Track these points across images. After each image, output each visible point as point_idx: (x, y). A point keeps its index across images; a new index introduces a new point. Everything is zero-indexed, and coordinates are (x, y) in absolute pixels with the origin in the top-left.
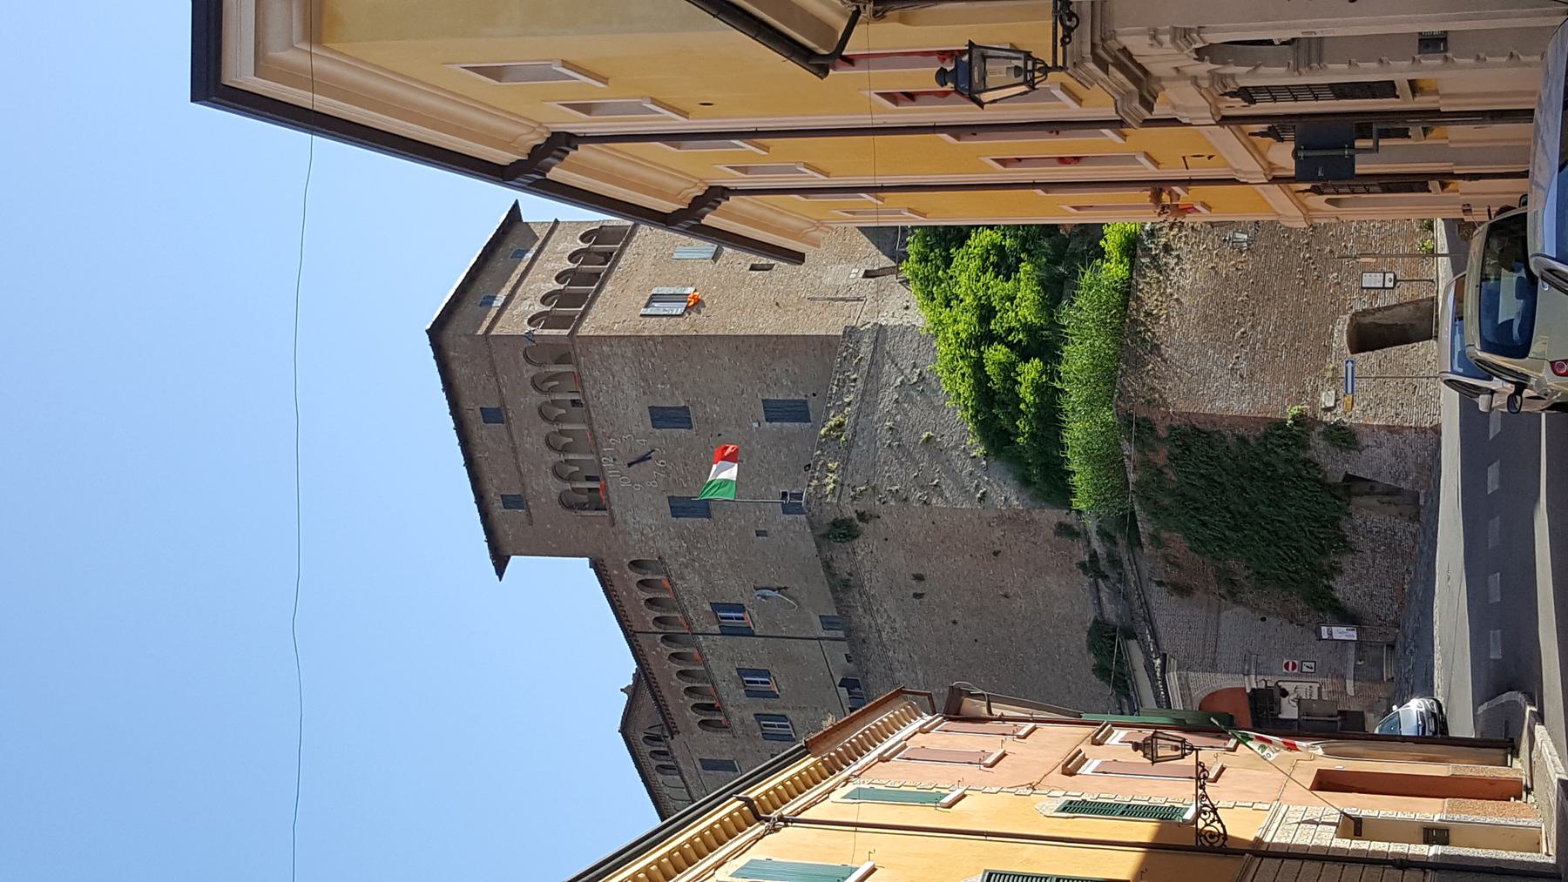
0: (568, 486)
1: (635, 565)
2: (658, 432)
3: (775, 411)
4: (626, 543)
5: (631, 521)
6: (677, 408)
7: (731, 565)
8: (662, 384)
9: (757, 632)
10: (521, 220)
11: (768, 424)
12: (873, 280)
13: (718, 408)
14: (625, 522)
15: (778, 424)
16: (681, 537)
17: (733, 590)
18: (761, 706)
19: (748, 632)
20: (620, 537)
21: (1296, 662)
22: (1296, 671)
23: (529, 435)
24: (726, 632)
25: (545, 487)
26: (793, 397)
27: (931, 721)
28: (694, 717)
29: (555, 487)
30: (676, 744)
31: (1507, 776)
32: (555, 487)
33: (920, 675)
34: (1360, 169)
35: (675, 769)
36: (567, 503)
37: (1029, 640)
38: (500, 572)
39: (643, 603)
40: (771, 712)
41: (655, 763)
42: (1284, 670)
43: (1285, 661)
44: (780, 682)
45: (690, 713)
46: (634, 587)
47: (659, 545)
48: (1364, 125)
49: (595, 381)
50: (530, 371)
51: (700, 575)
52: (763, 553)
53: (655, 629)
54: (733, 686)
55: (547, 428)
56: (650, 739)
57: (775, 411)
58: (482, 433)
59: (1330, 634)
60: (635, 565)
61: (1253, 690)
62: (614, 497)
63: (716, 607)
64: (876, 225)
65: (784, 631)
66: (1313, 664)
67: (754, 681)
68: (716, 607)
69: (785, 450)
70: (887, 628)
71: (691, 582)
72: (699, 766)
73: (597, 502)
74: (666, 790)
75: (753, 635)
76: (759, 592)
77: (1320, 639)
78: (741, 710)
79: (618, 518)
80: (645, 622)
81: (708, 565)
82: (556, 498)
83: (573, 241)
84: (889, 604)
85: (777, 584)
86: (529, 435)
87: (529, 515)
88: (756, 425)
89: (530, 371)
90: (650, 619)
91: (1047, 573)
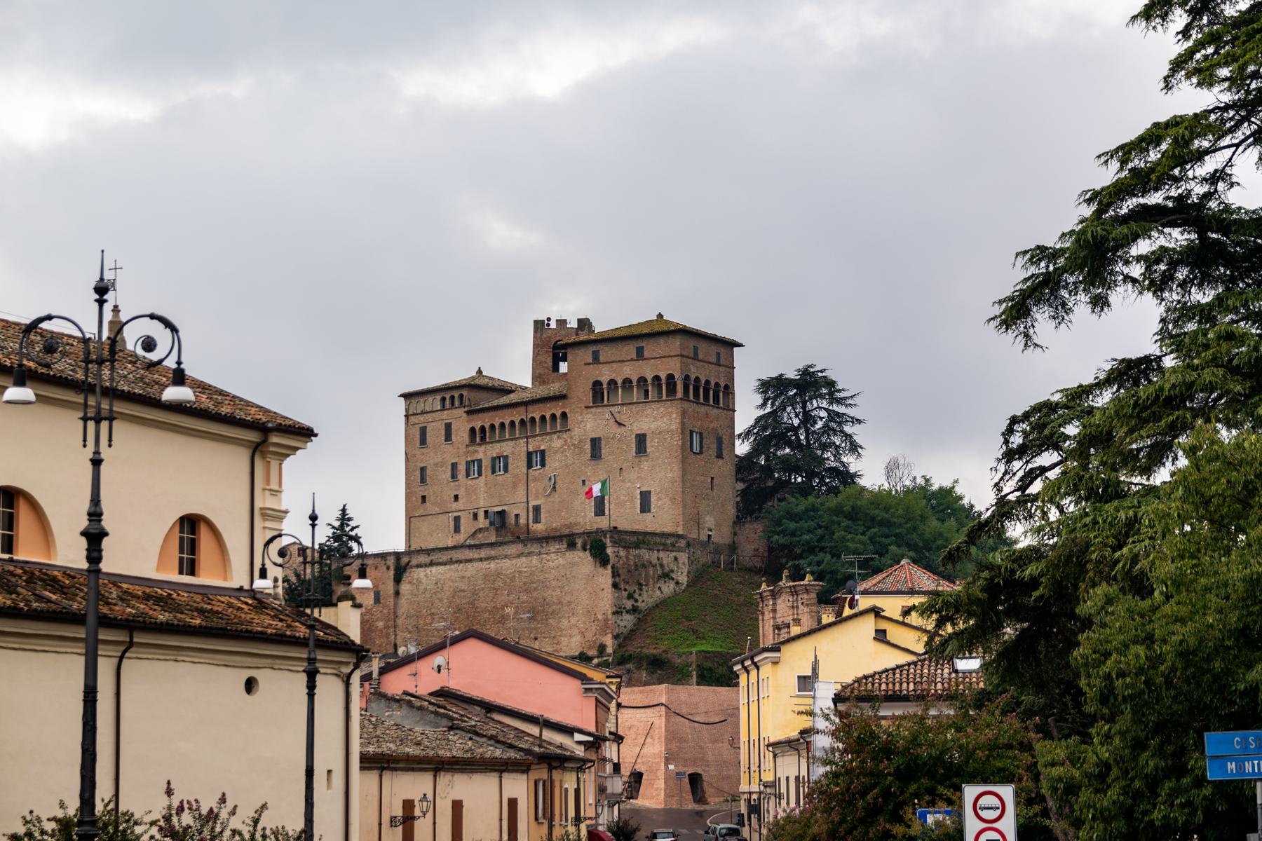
0: (605, 386)
1: (564, 415)
2: (634, 436)
3: (645, 497)
9: (530, 471)
15: (639, 497)
16: (581, 441)
17: (553, 463)
18: (486, 463)
19: (529, 466)
20: (579, 410)
24: (529, 455)
26: (653, 506)
27: (612, 691)
28: (478, 425)
29: (605, 380)
32: (605, 380)
34: (752, 816)
35: (443, 409)
36: (597, 384)
41: (448, 396)
44: (501, 477)
46: (552, 412)
48: (759, 816)
49: (659, 408)
53: (529, 417)
54: (497, 451)
55: (634, 380)
57: (645, 497)
58: (630, 350)
62: (600, 410)
63: (543, 452)
64: (743, 737)
65: (531, 485)
67: (502, 463)
68: (543, 452)
69: (626, 499)
70: (549, 558)
71: (556, 443)
72: (447, 421)
76: (553, 478)
78: (485, 453)
79: (589, 410)
80: (533, 412)
82: (599, 379)
84: (561, 561)
85: (557, 487)
87: (589, 364)
90: (534, 415)
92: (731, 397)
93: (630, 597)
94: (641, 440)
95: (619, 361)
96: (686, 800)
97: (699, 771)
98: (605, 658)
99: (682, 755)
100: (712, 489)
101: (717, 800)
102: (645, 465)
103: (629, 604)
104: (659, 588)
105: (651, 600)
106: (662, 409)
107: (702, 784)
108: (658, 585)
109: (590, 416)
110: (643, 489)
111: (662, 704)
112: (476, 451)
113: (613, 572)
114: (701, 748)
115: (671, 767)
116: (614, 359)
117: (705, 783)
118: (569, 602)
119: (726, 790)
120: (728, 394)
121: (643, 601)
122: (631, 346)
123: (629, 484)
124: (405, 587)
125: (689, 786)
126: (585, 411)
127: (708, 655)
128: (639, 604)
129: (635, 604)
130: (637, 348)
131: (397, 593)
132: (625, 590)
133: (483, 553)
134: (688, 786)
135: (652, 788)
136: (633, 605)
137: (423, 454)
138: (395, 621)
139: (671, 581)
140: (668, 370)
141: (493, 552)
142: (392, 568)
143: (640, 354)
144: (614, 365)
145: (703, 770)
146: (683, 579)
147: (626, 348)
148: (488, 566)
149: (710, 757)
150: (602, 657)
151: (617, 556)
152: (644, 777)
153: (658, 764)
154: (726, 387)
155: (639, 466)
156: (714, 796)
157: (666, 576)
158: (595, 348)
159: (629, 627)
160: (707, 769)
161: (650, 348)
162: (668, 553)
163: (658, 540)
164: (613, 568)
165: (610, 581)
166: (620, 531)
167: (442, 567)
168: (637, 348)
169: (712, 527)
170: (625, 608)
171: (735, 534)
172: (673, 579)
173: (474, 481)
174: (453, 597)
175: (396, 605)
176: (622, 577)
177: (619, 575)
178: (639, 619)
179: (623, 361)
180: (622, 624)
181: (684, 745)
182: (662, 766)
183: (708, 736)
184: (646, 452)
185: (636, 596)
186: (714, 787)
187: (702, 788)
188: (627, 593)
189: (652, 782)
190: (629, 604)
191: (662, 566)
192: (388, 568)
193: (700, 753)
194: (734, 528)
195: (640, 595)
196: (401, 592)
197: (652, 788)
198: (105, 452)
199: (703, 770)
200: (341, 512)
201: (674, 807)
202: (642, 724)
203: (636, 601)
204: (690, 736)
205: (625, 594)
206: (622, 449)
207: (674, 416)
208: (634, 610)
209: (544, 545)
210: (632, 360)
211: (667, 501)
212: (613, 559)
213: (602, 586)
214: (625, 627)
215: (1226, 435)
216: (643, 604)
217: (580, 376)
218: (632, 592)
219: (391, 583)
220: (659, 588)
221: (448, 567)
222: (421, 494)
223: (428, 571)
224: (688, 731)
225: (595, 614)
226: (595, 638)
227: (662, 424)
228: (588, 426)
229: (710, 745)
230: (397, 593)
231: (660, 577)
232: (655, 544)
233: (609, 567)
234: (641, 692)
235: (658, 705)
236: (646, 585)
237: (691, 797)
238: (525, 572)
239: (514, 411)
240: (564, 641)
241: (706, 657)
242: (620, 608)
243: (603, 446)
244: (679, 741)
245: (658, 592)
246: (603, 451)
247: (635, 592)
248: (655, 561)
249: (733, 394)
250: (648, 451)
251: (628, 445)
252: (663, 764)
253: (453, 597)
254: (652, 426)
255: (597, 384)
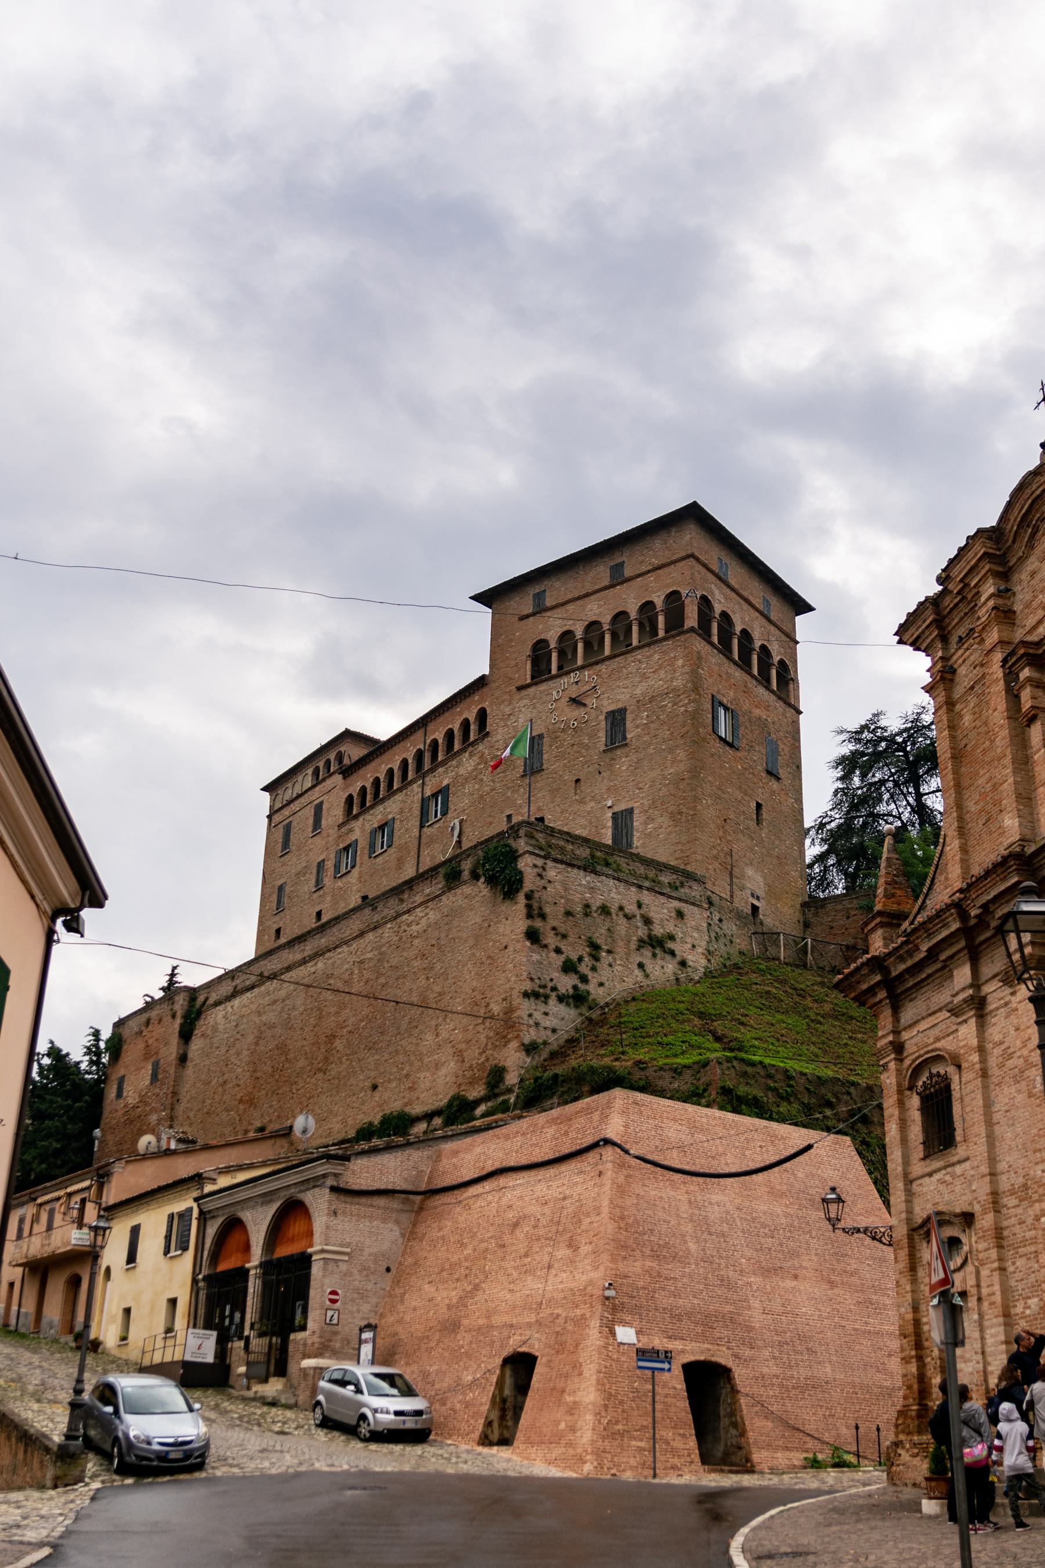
1: (482, 715)
2: (602, 717)
4: (503, 702)
5: (521, 704)
6: (625, 731)
7: (481, 797)
8: (648, 716)
10: (797, 615)
11: (610, 815)
12: (750, 912)
13: (624, 768)
14: (522, 699)
15: (610, 824)
18: (363, 844)
20: (506, 697)
21: (339, 1304)
22: (328, 1303)
23: (600, 606)
24: (424, 803)
25: (551, 628)
26: (636, 835)
28: (355, 789)
30: (338, 778)
31: (802, 1486)
32: (552, 637)
33: (369, 955)
36: (541, 645)
37: (397, 1052)
38: (478, 598)
39: (450, 726)
40: (359, 853)
42: (329, 1290)
43: (339, 1291)
45: (359, 785)
46: (464, 716)
47: (500, 731)
50: (659, 601)
51: (473, 771)
52: (491, 823)
53: (428, 741)
56: (340, 757)
58: (600, 573)
59: (366, 1341)
60: (482, 715)
61: (310, 1256)
62: (543, 687)
66: (335, 1321)
70: (411, 918)
73: (540, 671)
74: (300, 778)
75: (422, 826)
76: (457, 825)
77: (361, 1330)
78: (360, 830)
79: (524, 693)
80: (434, 733)
81: (481, 776)
83: (780, 653)
84: (433, 916)
86: (600, 606)
88: (609, 803)
89: (659, 601)
91: (457, 1061)
92: (791, 686)
93: (569, 967)
94: (617, 719)
95: (579, 598)
96: (674, 1452)
97: (723, 1358)
98: (501, 1098)
99: (664, 1300)
100: (759, 821)
101: (781, 1458)
102: (623, 762)
103: (566, 983)
104: (641, 966)
105: (619, 987)
106: (657, 656)
107: (735, 1402)
108: (639, 959)
109: (525, 701)
110: (616, 809)
111: (607, 1142)
112: (351, 830)
113: (529, 907)
114: (725, 1282)
115: (626, 1334)
116: (570, 596)
117: (743, 1401)
118: (440, 994)
119: (810, 1428)
120: (787, 684)
121: (601, 984)
122: (601, 568)
123: (592, 804)
124: (196, 1045)
125: (685, 1404)
126: (517, 696)
127: (750, 1070)
128: (592, 987)
129: (582, 987)
130: (612, 568)
131: (183, 1059)
132: (558, 951)
133: (308, 948)
134: (683, 1404)
135: (559, 1402)
136: (575, 987)
137: (284, 864)
138: (172, 1109)
139: (668, 957)
140: (667, 586)
141: (322, 941)
142: (179, 1014)
143: (618, 579)
144: (570, 607)
145: (736, 1356)
146: (698, 961)
147: (592, 574)
148: (313, 970)
149: (757, 1317)
150: (496, 1096)
151: (540, 875)
152: (539, 1370)
153: (581, 1322)
154: (783, 666)
155: (610, 767)
156: (769, 1446)
157: (657, 944)
158: (537, 589)
159: (563, 1036)
160: (748, 1353)
161: (633, 561)
162: (662, 899)
163: (641, 870)
164: (529, 896)
165: (521, 925)
166: (552, 832)
167: (248, 994)
168: (612, 568)
169: (760, 893)
170: (554, 989)
171: (806, 925)
172: (672, 953)
173: (344, 879)
174: (257, 1044)
175: (178, 1080)
176: (552, 922)
177: (543, 916)
178: (590, 1020)
179: (587, 595)
180: (547, 1022)
181: (673, 1269)
182: (593, 1335)
183: (748, 1253)
184: (625, 738)
185: (584, 969)
186: (768, 1415)
187: (734, 1412)
188: (562, 958)
189: (560, 1385)
190: (566, 983)
191: (647, 921)
192: (174, 1016)
193: (727, 1301)
194: (804, 914)
195: (594, 969)
196: (190, 1055)
197: (559, 1402)
198: (200, 1142)
199: (736, 1356)
200: (168, 978)
201: (628, 1476)
202: (546, 1210)
203: (584, 979)
204: (692, 1246)
205: (558, 960)
206: (580, 744)
207: (680, 662)
208: (578, 998)
209: (406, 896)
210: (606, 588)
211: (664, 820)
212: (530, 882)
213: (504, 941)
214: (554, 1031)
215: (916, 1438)
216: (601, 991)
217: (511, 641)
218: (574, 957)
219: (175, 1040)
220: (641, 966)
221: (256, 990)
222: (276, 927)
223: (229, 1009)
224: (689, 1228)
225: (488, 1005)
226: (483, 1059)
227: (657, 682)
228: (521, 721)
229: (756, 1280)
230: (183, 1059)
231: (642, 944)
232: (632, 873)
233: (521, 898)
234: (554, 1121)
235: (595, 1146)
236: (609, 952)
237: (692, 1443)
238: (370, 959)
239: (407, 743)
240: (425, 1079)
241: (745, 1074)
242: (544, 987)
243: (545, 748)
244: (656, 1256)
245: (637, 972)
246: (545, 757)
247: (580, 959)
248: (631, 908)
249: (795, 680)
250: (629, 736)
251: (592, 736)
252: (595, 1323)
253: (257, 1044)
254: (638, 691)
255: (541, 645)
